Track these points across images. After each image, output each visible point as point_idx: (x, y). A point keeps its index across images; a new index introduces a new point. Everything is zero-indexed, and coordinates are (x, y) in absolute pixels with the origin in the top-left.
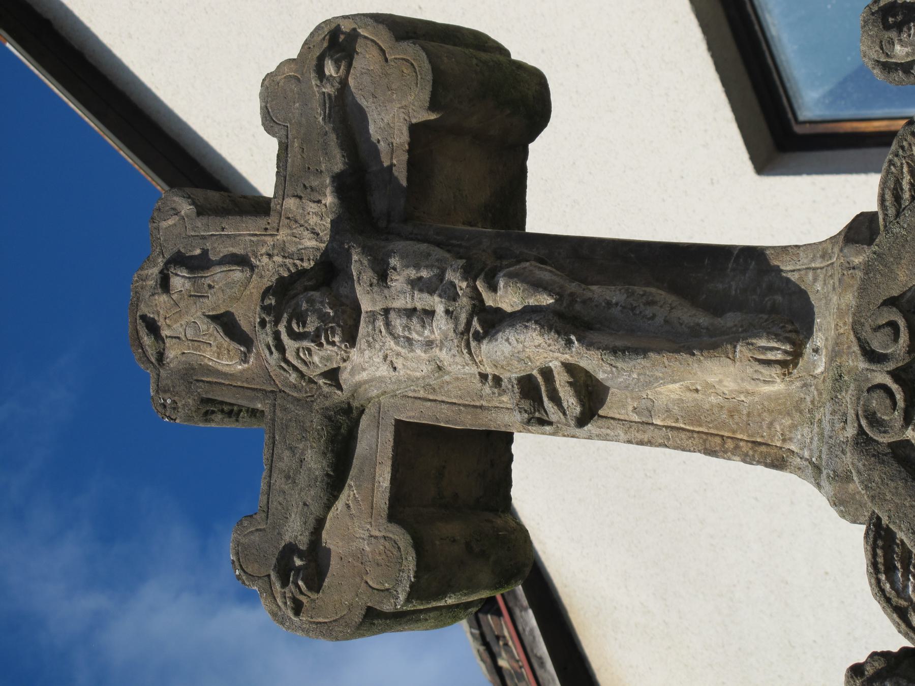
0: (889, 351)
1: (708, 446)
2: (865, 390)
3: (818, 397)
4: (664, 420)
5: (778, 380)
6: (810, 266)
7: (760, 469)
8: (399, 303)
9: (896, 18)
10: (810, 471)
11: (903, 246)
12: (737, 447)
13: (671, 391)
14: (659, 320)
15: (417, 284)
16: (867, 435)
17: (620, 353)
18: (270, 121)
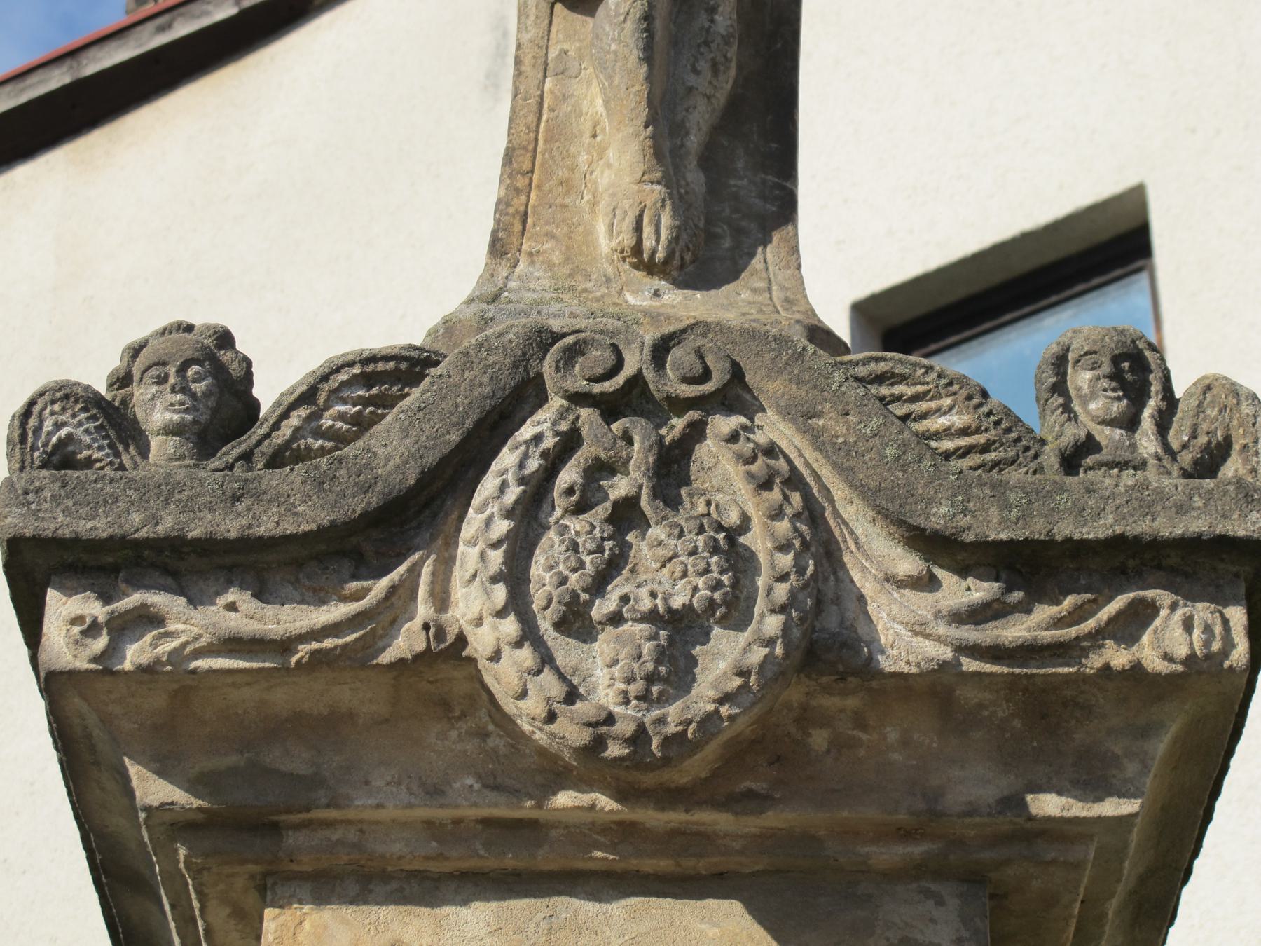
0: (669, 371)
1: (518, 152)
2: (615, 341)
3: (592, 298)
4: (551, 92)
5: (614, 244)
6: (773, 284)
7: (489, 224)
9: (1128, 371)
10: (490, 289)
11: (815, 386)
12: (518, 191)
13: (592, 102)
14: (692, 80)
16: (552, 344)
17: (645, 25)
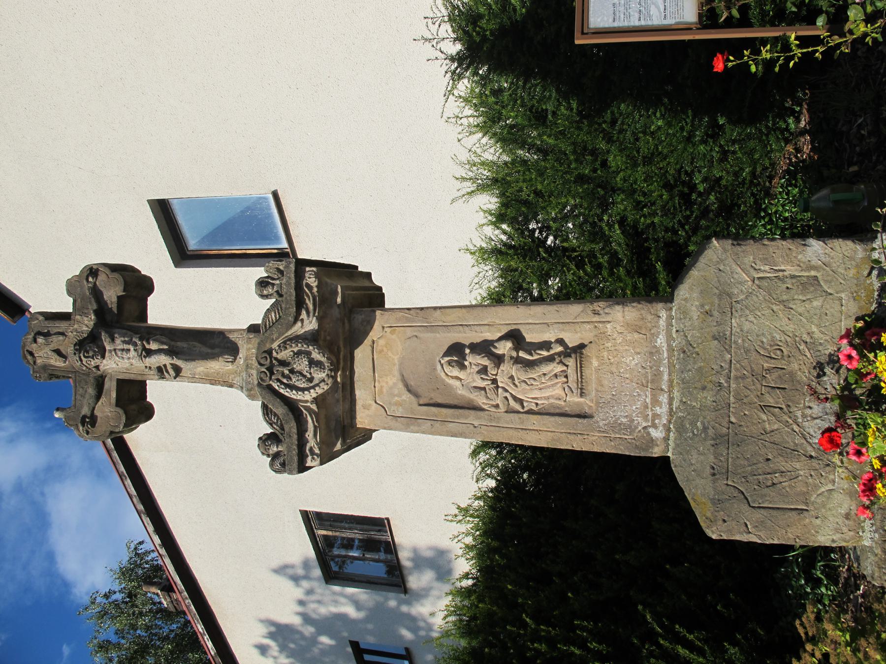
8: (121, 347)
10: (240, 388)
15: (124, 342)
18: (69, 293)
